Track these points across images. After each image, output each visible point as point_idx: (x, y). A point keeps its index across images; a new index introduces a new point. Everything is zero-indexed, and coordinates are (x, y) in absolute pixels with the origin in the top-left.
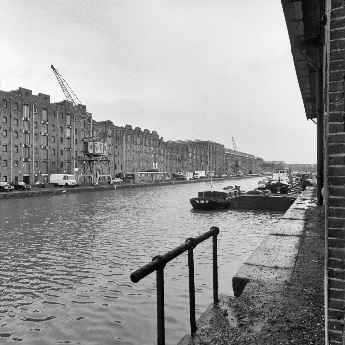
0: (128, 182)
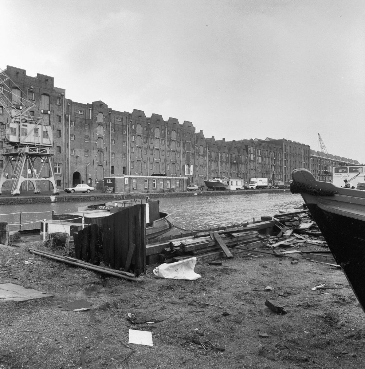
0: (105, 191)
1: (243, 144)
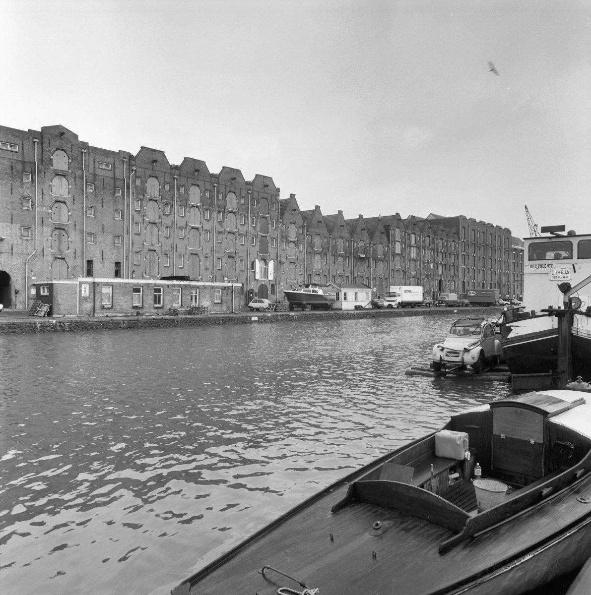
1: (380, 222)
